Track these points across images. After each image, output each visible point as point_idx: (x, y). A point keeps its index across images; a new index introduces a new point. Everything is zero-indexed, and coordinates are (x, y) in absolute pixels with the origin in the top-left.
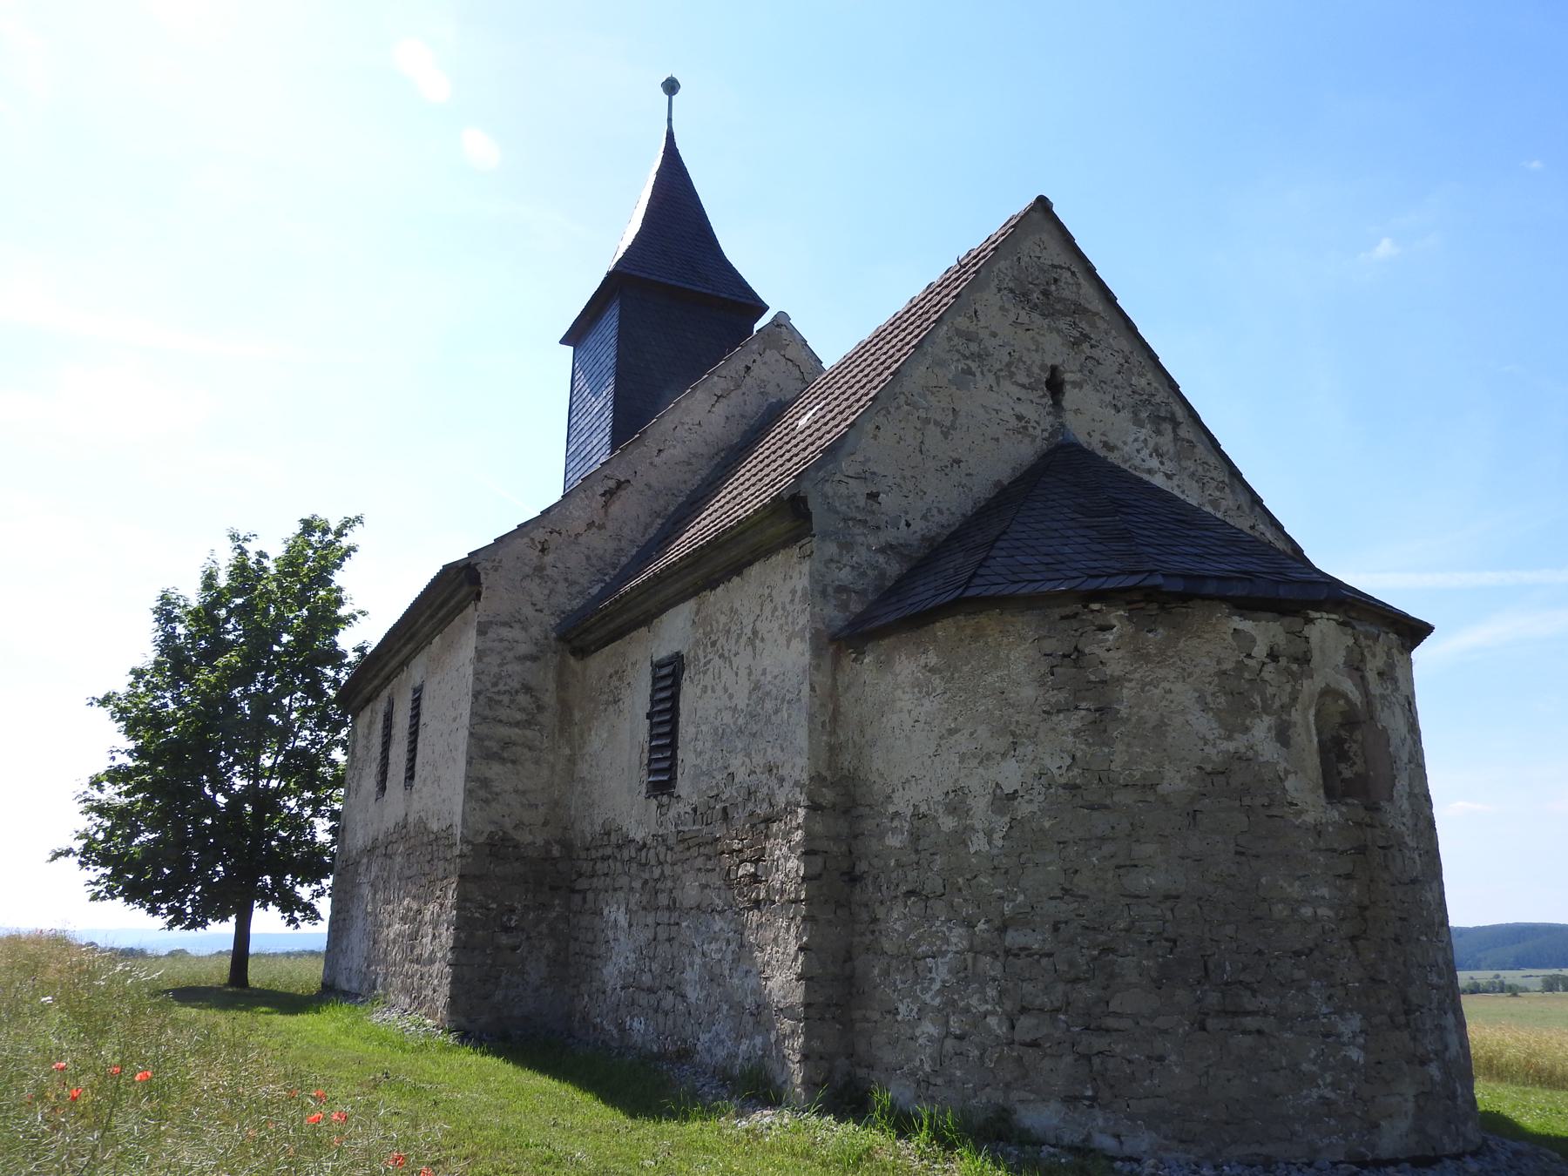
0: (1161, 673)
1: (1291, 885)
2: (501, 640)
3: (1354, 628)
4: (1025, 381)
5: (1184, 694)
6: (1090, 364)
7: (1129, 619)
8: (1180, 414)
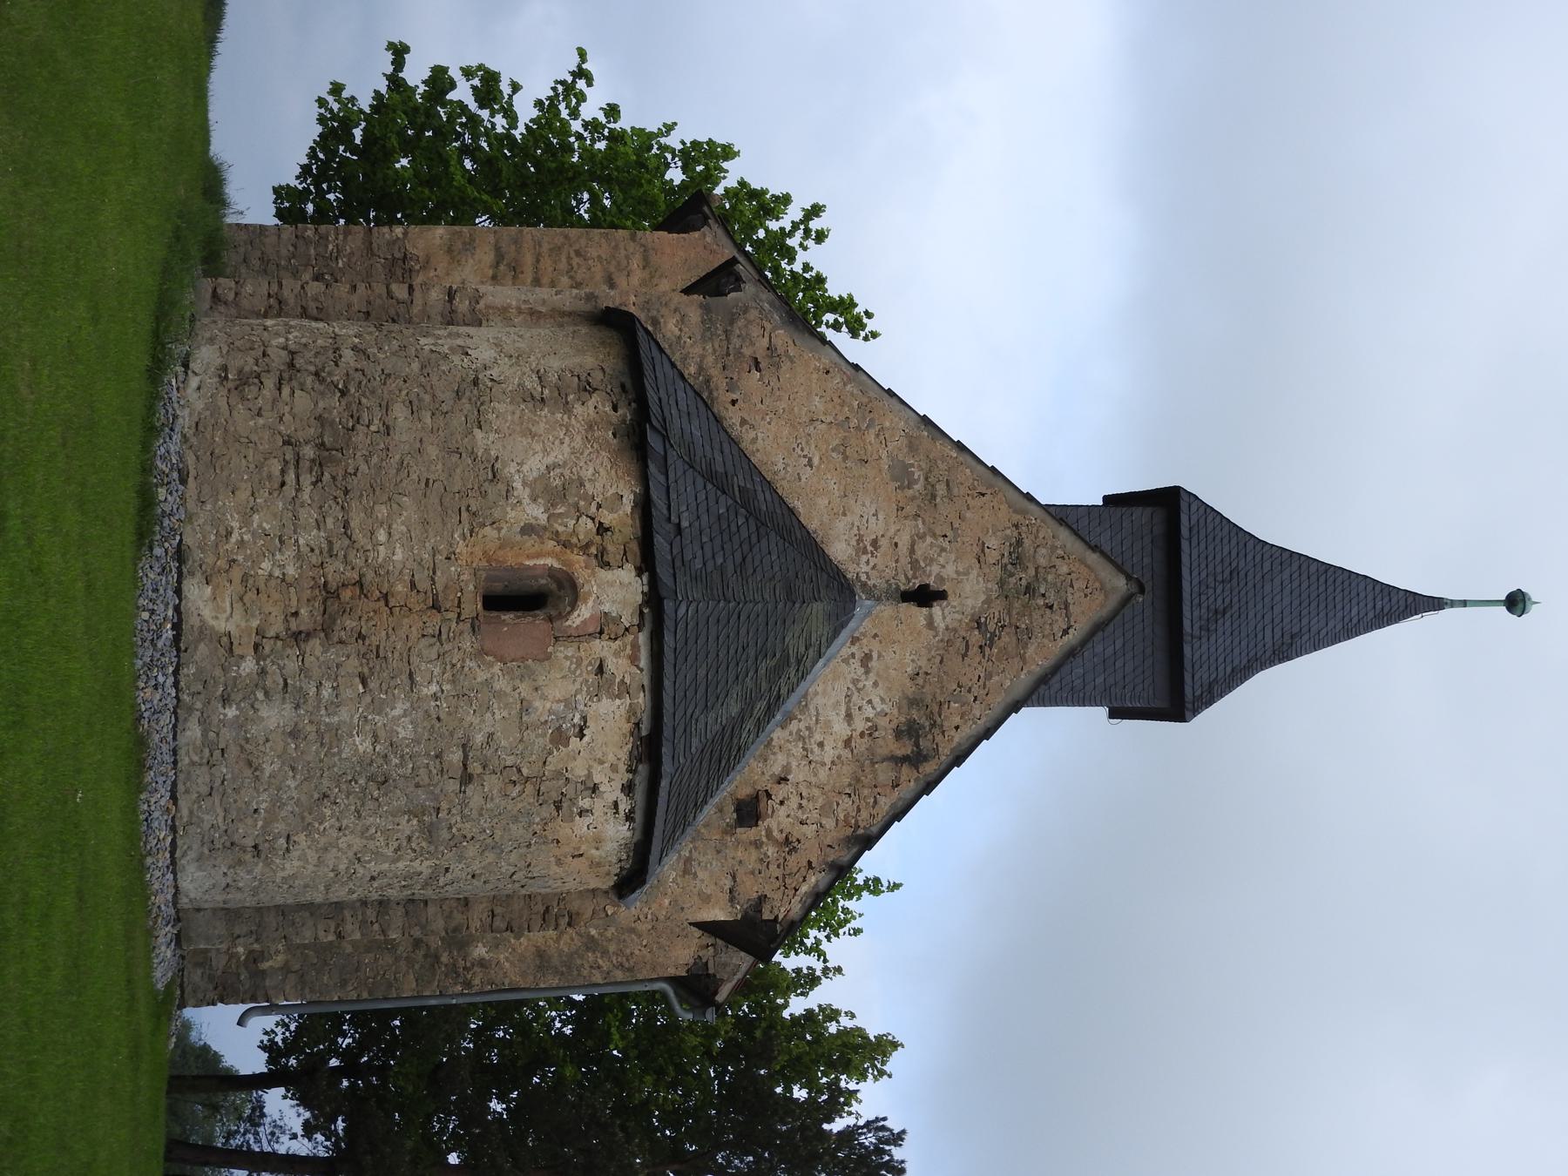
0: (578, 439)
1: (403, 523)
2: (627, 257)
3: (640, 627)
4: (919, 554)
5: (560, 454)
6: (960, 644)
7: (624, 421)
8: (929, 768)
